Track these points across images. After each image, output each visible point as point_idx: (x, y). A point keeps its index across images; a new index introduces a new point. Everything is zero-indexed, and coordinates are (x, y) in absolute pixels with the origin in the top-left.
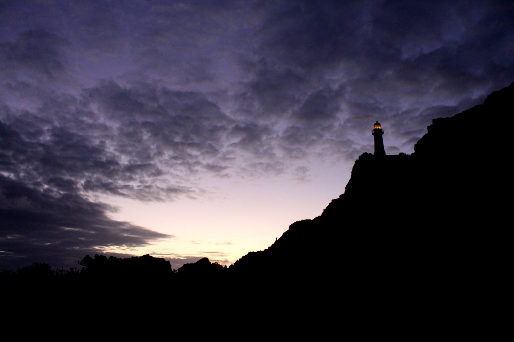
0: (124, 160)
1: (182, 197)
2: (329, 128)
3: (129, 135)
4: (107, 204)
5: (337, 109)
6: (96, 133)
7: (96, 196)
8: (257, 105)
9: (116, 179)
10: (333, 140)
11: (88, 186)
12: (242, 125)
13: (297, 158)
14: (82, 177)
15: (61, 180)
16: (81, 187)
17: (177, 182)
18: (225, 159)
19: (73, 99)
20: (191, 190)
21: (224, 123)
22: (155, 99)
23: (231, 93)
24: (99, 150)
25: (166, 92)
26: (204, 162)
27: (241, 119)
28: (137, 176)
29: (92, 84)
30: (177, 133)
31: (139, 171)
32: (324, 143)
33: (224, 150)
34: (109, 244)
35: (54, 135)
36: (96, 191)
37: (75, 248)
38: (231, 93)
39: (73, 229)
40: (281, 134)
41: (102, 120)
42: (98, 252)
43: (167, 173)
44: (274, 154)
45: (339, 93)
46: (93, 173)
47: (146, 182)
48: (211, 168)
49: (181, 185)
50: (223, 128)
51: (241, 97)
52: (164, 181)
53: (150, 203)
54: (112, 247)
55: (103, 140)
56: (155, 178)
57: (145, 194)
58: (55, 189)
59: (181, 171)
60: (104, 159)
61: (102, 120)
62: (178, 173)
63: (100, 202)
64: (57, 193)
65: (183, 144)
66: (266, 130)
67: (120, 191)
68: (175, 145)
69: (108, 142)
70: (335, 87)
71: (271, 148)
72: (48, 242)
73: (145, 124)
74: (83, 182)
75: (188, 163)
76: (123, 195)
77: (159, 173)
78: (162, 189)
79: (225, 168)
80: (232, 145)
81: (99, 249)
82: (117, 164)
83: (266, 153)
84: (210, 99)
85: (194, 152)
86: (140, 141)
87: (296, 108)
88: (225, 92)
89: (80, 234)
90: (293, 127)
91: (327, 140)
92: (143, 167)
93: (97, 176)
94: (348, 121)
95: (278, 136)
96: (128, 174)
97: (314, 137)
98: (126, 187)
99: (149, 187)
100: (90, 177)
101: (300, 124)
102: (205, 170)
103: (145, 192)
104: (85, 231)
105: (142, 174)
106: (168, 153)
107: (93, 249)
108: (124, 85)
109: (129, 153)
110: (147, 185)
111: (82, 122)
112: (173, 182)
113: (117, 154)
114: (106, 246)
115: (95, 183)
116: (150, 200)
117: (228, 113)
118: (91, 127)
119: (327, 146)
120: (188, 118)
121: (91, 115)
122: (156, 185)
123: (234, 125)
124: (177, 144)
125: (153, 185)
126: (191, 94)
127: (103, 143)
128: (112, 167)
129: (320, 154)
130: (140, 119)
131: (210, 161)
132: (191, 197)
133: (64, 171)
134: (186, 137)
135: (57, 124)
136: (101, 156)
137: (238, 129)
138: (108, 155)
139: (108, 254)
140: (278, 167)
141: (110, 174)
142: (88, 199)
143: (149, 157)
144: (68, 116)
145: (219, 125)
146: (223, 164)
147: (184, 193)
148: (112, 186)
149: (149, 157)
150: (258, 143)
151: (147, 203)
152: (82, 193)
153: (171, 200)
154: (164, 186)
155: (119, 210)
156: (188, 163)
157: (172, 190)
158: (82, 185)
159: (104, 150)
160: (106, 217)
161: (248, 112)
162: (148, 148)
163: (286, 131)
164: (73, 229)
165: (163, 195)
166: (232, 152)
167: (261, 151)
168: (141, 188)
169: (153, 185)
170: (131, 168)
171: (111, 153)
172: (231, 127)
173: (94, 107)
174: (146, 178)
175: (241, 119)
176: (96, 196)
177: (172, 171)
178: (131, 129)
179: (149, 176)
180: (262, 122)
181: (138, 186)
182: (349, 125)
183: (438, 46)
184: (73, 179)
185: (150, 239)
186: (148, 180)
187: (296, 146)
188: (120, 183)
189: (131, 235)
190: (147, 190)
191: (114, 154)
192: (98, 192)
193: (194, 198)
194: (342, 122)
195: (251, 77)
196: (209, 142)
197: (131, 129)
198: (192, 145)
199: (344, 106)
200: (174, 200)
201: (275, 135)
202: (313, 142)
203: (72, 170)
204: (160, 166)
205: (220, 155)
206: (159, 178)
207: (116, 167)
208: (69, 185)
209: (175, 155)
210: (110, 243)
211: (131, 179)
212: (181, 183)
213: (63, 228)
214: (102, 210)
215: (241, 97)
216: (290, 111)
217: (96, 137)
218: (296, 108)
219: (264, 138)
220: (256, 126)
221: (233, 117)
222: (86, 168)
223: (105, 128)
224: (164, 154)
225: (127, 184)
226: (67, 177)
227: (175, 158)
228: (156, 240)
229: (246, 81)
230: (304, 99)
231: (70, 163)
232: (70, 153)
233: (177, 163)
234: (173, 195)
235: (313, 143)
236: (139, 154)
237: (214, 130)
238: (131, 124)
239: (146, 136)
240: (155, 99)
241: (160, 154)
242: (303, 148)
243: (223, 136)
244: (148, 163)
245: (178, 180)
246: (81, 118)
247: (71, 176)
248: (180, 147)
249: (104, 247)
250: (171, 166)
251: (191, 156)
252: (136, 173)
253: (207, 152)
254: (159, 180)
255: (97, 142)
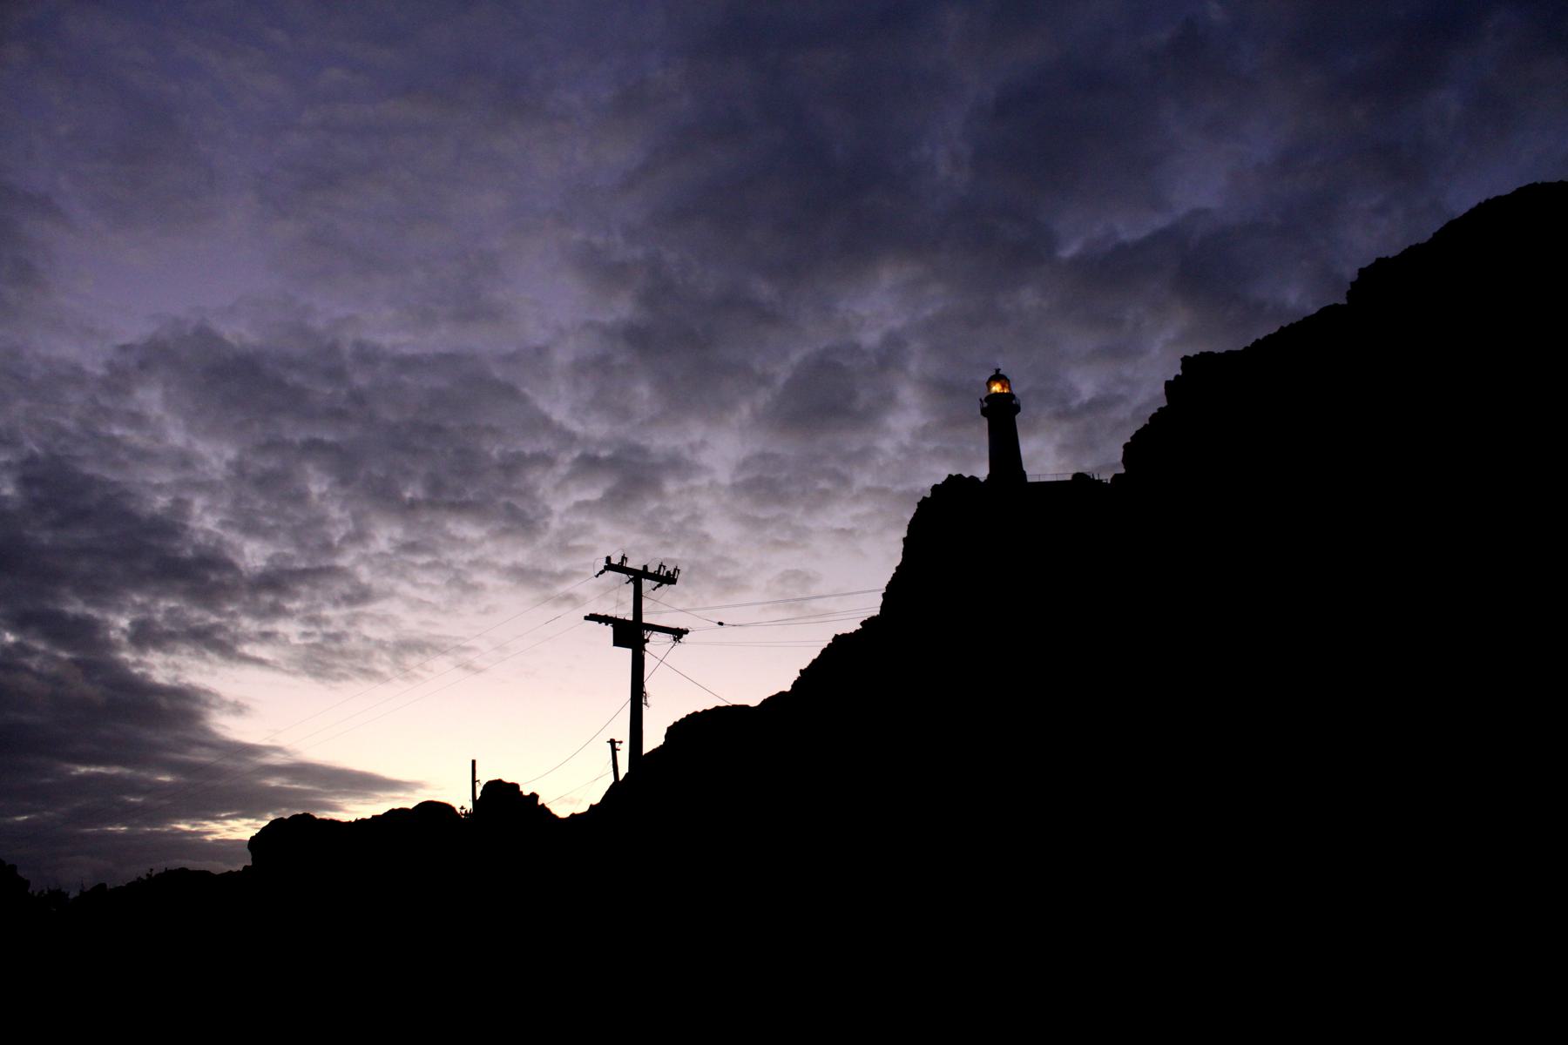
0: (254, 555)
1: (441, 663)
2: (864, 456)
3: (266, 482)
4: (213, 691)
5: (888, 400)
6: (164, 476)
7: (176, 667)
8: (643, 391)
9: (233, 614)
10: (882, 492)
11: (144, 636)
12: (604, 453)
13: (778, 544)
14: (120, 610)
15: (59, 617)
16: (124, 639)
17: (423, 623)
18: (564, 549)
19: (76, 376)
20: (466, 644)
21: (546, 444)
22: (336, 374)
23: (562, 357)
24: (169, 526)
25: (367, 356)
26: (506, 561)
27: (597, 429)
28: (296, 605)
29: (136, 330)
30: (408, 474)
31: (304, 589)
32: (857, 499)
33: (555, 523)
34: (223, 815)
35: (26, 482)
36: (172, 651)
37: (184, 826)
38: (562, 357)
39: (101, 770)
40: (724, 477)
41: (177, 437)
42: (189, 838)
43: (390, 594)
44: (706, 537)
45: (891, 354)
46: (159, 594)
47: (328, 621)
48: (523, 575)
49: (435, 631)
50: (547, 460)
51: (599, 366)
52: (384, 620)
53: (344, 684)
54: (232, 823)
55: (186, 496)
56: (357, 609)
57: (328, 660)
58: (41, 646)
59: (427, 587)
60: (189, 553)
61: (177, 437)
62: (426, 595)
63: (189, 685)
64: (47, 656)
65: (431, 505)
66: (677, 465)
67: (247, 649)
68: (408, 509)
69: (199, 502)
70: (871, 338)
71: (695, 518)
72: (23, 813)
73: (313, 447)
74: (124, 622)
75: (448, 566)
76: (260, 662)
77: (362, 595)
78: (381, 645)
79: (564, 576)
80: (581, 506)
81: (194, 829)
82: (230, 566)
83: (680, 530)
84: (498, 373)
85: (467, 529)
86: (301, 498)
87: (763, 397)
88: (541, 351)
89: (131, 786)
90: (764, 457)
91: (868, 490)
92: (317, 574)
93: (165, 606)
94: (924, 433)
95: (712, 484)
96: (267, 598)
97: (824, 484)
98: (267, 637)
99: (337, 637)
100: (143, 607)
101: (787, 447)
102: (506, 583)
103: (331, 653)
104: (144, 774)
105: (313, 598)
106: (386, 535)
107: (177, 832)
108: (239, 333)
109: (266, 534)
110: (331, 630)
111: (114, 442)
112: (412, 623)
113: (232, 536)
114: (214, 819)
115: (166, 627)
116: (342, 677)
117: (560, 414)
118: (142, 455)
119: (864, 509)
120: (437, 429)
121: (137, 420)
122: (359, 634)
123: (576, 453)
124: (413, 505)
125: (351, 630)
126: (450, 360)
127: (181, 506)
128: (214, 577)
129: (844, 533)
130: (297, 432)
131: (518, 554)
132: (467, 667)
133: (66, 591)
134: (435, 486)
135: (32, 447)
136: (177, 544)
137: (589, 464)
138: (200, 538)
139: (222, 844)
140: (720, 574)
141: (208, 595)
142: (150, 676)
143: (328, 548)
144: (69, 424)
145: (528, 448)
146: (560, 565)
147: (445, 653)
148: (220, 636)
149: (328, 548)
150: (653, 505)
151: (334, 684)
152: (127, 656)
153: (407, 674)
154: (386, 634)
155: (247, 707)
156: (448, 566)
157: (408, 647)
158: (124, 631)
159: (185, 527)
160: (206, 731)
161: (624, 414)
162: (321, 520)
163: (744, 465)
164: (101, 770)
165: (383, 663)
166: (583, 530)
167: (666, 526)
168: (317, 639)
169: (351, 630)
170: (276, 582)
171: (208, 533)
172: (567, 459)
173: (150, 397)
174: (329, 612)
175: (597, 429)
176: (176, 667)
177: (404, 587)
178: (271, 462)
179: (336, 604)
180: (661, 441)
181: (305, 635)
182: (929, 446)
183: (1160, 221)
184: (93, 612)
185: (347, 794)
186: (335, 615)
187: (773, 511)
188: (248, 624)
189: (118, 776)
190: (335, 646)
191: (219, 541)
192: (180, 654)
193: (478, 671)
194: (906, 440)
195: (622, 308)
196: (504, 499)
197: (271, 462)
198: (461, 507)
199: (907, 393)
200: (416, 676)
201: (702, 481)
202: (824, 498)
203: (99, 589)
204: (365, 575)
205: (542, 541)
206: (370, 608)
207: (228, 577)
208: (83, 633)
209: (411, 539)
210: (222, 811)
211: (277, 611)
212: (436, 625)
213: (66, 766)
214: (197, 707)
215: (599, 366)
216: (745, 410)
217: (159, 488)
218: (763, 397)
219: (671, 486)
220: (641, 451)
221: (576, 427)
222: (139, 580)
223: (184, 460)
224: (373, 537)
225: (267, 628)
226: (75, 607)
227: (411, 548)
228: (374, 797)
229: (608, 318)
230: (782, 373)
231: (84, 565)
232: (84, 534)
233: (414, 565)
234: (413, 660)
235: (823, 499)
236: (298, 535)
237: (513, 466)
238: (271, 446)
239: (317, 484)
240: (336, 374)
241: (359, 536)
242: (798, 515)
243: (543, 483)
244: (324, 562)
245: (425, 615)
246: (103, 429)
247: (88, 603)
248: (425, 518)
249: (205, 823)
250: (402, 575)
251: (462, 543)
252: (295, 596)
253: (506, 532)
254: (371, 616)
255: (161, 502)
